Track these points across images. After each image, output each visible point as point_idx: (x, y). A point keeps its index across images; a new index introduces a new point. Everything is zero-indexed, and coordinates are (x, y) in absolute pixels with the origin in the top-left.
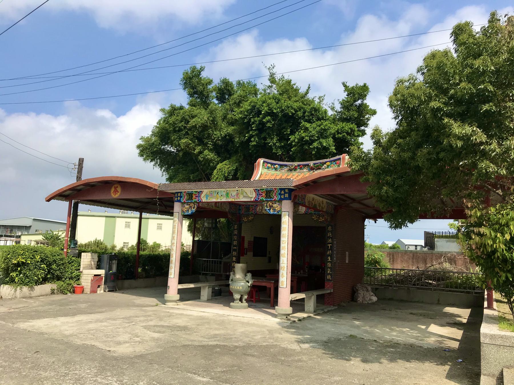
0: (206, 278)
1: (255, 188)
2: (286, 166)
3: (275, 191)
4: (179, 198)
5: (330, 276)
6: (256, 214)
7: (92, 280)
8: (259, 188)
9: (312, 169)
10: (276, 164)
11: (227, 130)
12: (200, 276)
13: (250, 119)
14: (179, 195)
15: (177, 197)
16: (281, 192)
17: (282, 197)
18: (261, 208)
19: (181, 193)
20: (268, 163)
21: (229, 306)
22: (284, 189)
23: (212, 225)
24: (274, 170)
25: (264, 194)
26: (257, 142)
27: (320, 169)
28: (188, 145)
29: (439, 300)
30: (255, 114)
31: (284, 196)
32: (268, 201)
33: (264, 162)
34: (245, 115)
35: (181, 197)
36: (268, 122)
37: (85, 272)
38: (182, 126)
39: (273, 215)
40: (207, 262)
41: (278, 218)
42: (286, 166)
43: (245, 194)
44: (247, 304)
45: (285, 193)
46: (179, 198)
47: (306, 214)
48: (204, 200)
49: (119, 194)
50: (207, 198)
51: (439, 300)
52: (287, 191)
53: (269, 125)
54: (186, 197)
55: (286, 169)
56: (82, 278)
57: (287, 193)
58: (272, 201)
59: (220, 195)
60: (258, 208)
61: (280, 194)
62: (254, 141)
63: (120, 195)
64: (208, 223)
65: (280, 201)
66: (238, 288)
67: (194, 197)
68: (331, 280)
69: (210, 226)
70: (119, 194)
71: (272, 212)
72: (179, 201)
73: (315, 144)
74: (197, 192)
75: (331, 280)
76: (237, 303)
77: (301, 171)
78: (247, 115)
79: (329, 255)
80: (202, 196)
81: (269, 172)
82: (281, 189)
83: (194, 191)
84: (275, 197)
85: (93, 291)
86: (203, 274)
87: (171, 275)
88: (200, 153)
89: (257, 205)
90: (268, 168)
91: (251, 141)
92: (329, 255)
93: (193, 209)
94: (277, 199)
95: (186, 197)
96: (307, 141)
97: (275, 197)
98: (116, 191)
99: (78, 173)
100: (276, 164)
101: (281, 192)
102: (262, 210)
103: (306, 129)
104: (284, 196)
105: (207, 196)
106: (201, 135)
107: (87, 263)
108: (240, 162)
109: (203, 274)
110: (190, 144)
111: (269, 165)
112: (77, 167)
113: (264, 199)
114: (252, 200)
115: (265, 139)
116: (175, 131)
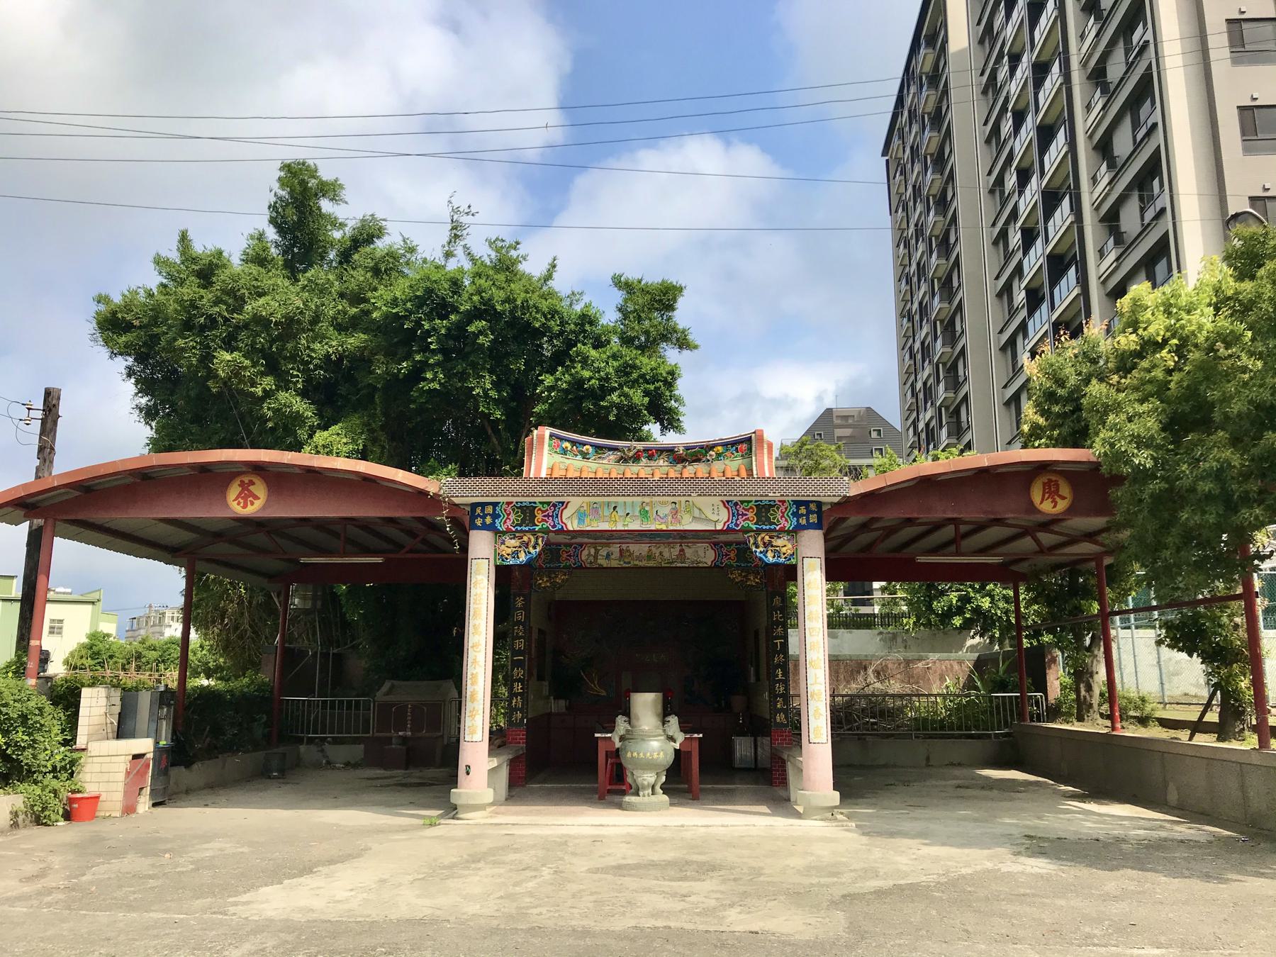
0: (322, 751)
1: (725, 499)
2: (615, 449)
3: (783, 508)
4: (488, 520)
5: (783, 716)
6: (581, 567)
7: (128, 773)
8: (735, 499)
9: (624, 460)
10: (584, 444)
11: (333, 344)
12: (303, 748)
13: (418, 324)
14: (489, 509)
15: (484, 517)
16: (798, 509)
17: (803, 521)
18: (593, 551)
19: (495, 505)
20: (562, 439)
21: (620, 806)
22: (806, 504)
23: (314, 605)
24: (579, 457)
25: (751, 515)
26: (440, 384)
27: (698, 460)
28: (237, 371)
29: (928, 759)
30: (432, 310)
31: (808, 519)
32: (759, 531)
33: (551, 436)
34: (406, 310)
35: (495, 516)
36: (481, 332)
37: (96, 748)
38: (220, 314)
39: (776, 565)
40: (333, 707)
41: (791, 572)
42: (615, 449)
43: (697, 513)
44: (666, 798)
45: (809, 512)
46: (488, 520)
47: (716, 566)
48: (573, 525)
49: (258, 504)
50: (581, 520)
51: (928, 759)
52: (813, 507)
53: (481, 340)
54: (512, 517)
55: (612, 456)
56: (87, 768)
57: (813, 512)
58: (775, 530)
59: (621, 511)
60: (585, 553)
61: (796, 515)
62: (433, 380)
63: (264, 508)
64: (304, 598)
65: (794, 533)
66: (655, 756)
67: (539, 516)
68: (787, 725)
69: (309, 605)
70: (258, 504)
71: (770, 558)
72: (491, 528)
73: (614, 397)
74: (548, 503)
75: (787, 725)
76: (644, 798)
77: (652, 463)
78: (411, 312)
79: (778, 666)
80: (566, 514)
81: (568, 462)
82: (798, 504)
83: (537, 500)
84: (783, 521)
85: (129, 809)
86: (311, 741)
87: (473, 733)
88: (268, 394)
89: (581, 545)
90: (565, 452)
91: (425, 379)
92: (778, 666)
93: (533, 551)
94: (787, 526)
95: (512, 517)
96: (592, 389)
97: (783, 521)
98: (246, 495)
99: (43, 432)
100: (584, 444)
101: (798, 509)
102: (596, 557)
103: (585, 361)
104: (808, 519)
105: (581, 516)
106: (276, 344)
107: (96, 720)
108: (371, 431)
109: (311, 741)
110: (245, 368)
111: (568, 445)
112: (39, 414)
113: (754, 527)
114: (719, 527)
115: (463, 377)
116: (188, 326)
